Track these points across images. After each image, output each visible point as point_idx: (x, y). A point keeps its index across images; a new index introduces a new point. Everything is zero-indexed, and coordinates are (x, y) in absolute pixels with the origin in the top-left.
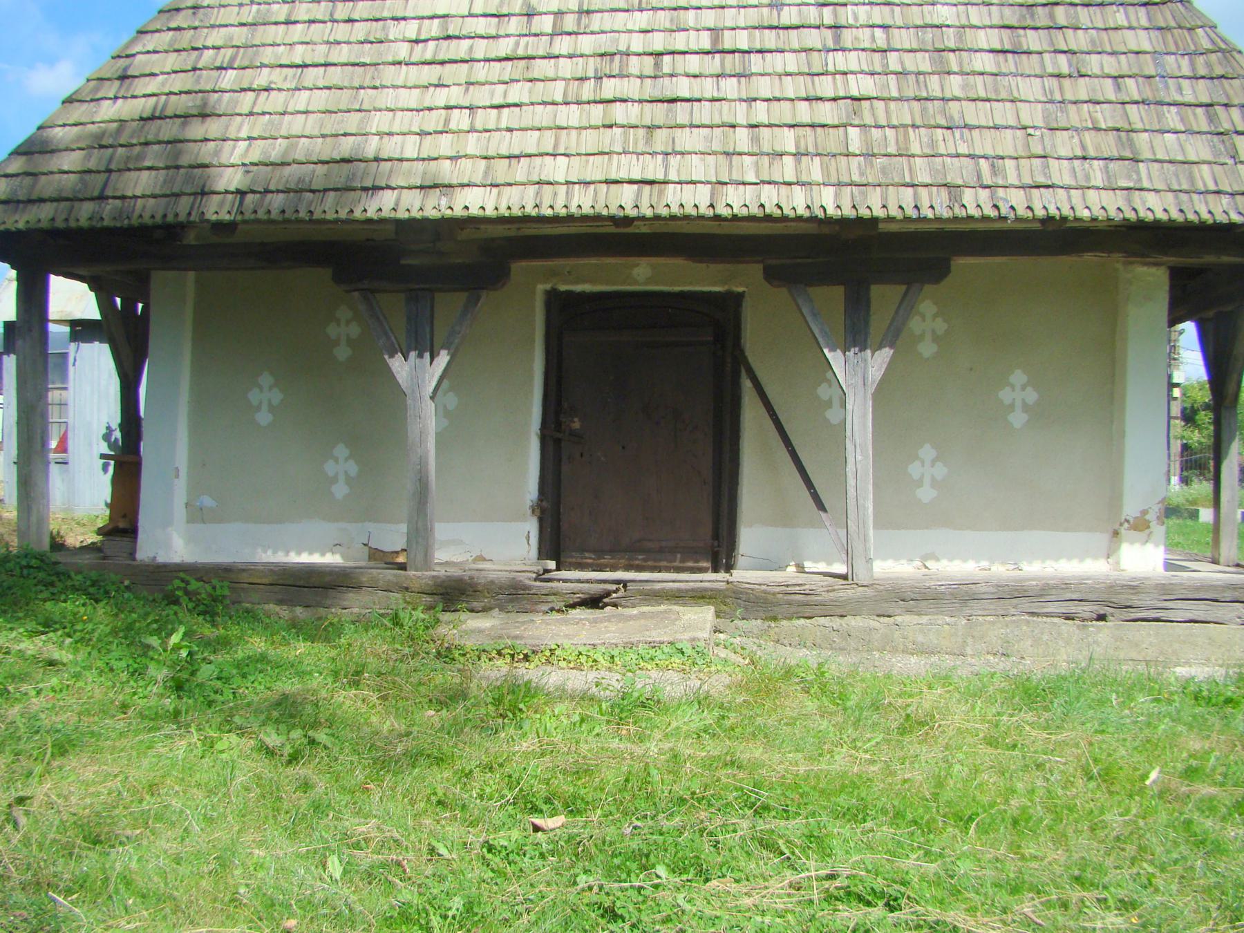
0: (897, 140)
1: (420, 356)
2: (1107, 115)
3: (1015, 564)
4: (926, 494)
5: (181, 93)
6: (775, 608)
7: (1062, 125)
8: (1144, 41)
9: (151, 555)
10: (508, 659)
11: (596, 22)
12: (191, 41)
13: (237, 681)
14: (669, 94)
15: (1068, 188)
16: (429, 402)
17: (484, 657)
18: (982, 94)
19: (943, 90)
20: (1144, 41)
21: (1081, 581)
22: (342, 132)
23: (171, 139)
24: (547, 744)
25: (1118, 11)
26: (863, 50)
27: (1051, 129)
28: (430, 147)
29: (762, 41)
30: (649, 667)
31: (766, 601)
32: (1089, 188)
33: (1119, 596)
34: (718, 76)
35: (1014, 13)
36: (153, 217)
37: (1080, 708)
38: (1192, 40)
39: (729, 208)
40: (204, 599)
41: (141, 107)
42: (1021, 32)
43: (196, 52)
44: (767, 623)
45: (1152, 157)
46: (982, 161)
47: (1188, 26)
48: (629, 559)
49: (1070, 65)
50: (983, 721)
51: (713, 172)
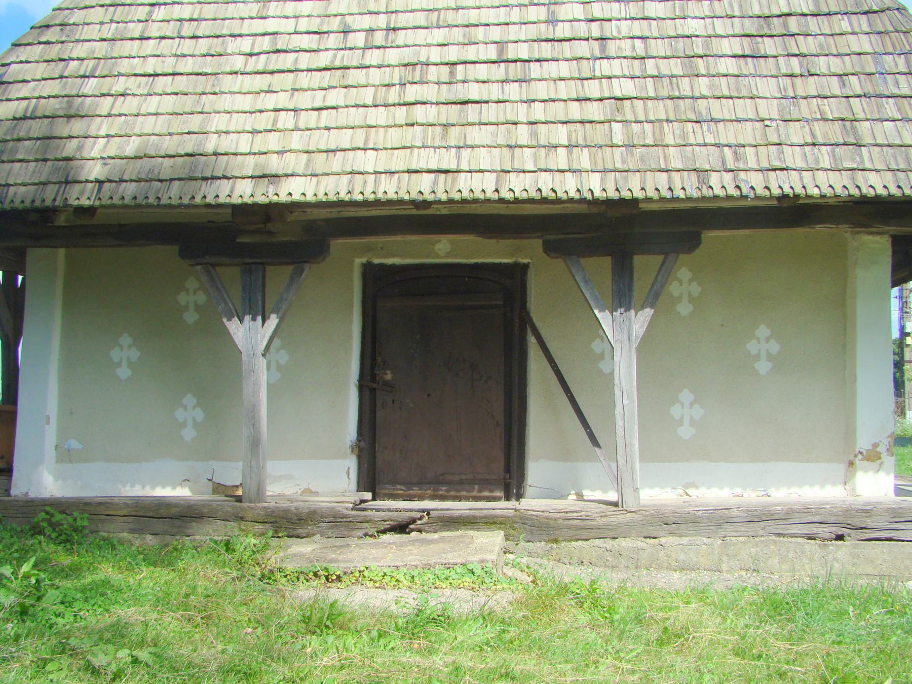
0: (654, 133)
1: (254, 319)
2: (833, 106)
3: (765, 491)
4: (686, 432)
5: (49, 97)
6: (556, 532)
7: (794, 117)
8: (865, 44)
9: (24, 491)
10: (323, 580)
11: (401, 37)
12: (58, 54)
13: (77, 605)
14: (462, 98)
15: (799, 170)
16: (261, 358)
17: (302, 578)
18: (726, 92)
19: (692, 90)
20: (865, 44)
21: (820, 507)
22: (187, 131)
23: (40, 136)
24: (346, 659)
25: (843, 19)
26: (625, 58)
27: (785, 121)
28: (261, 142)
29: (540, 51)
30: (444, 586)
31: (548, 526)
32: (818, 170)
33: (854, 519)
34: (503, 82)
35: (753, 23)
36: (23, 202)
37: (819, 620)
38: (907, 41)
39: (511, 193)
40: (66, 530)
41: (14, 109)
42: (759, 39)
43: (63, 63)
44: (550, 545)
45: (873, 142)
46: (726, 149)
47: (904, 29)
48: (434, 490)
49: (801, 66)
50: (733, 632)
51: (498, 162)
